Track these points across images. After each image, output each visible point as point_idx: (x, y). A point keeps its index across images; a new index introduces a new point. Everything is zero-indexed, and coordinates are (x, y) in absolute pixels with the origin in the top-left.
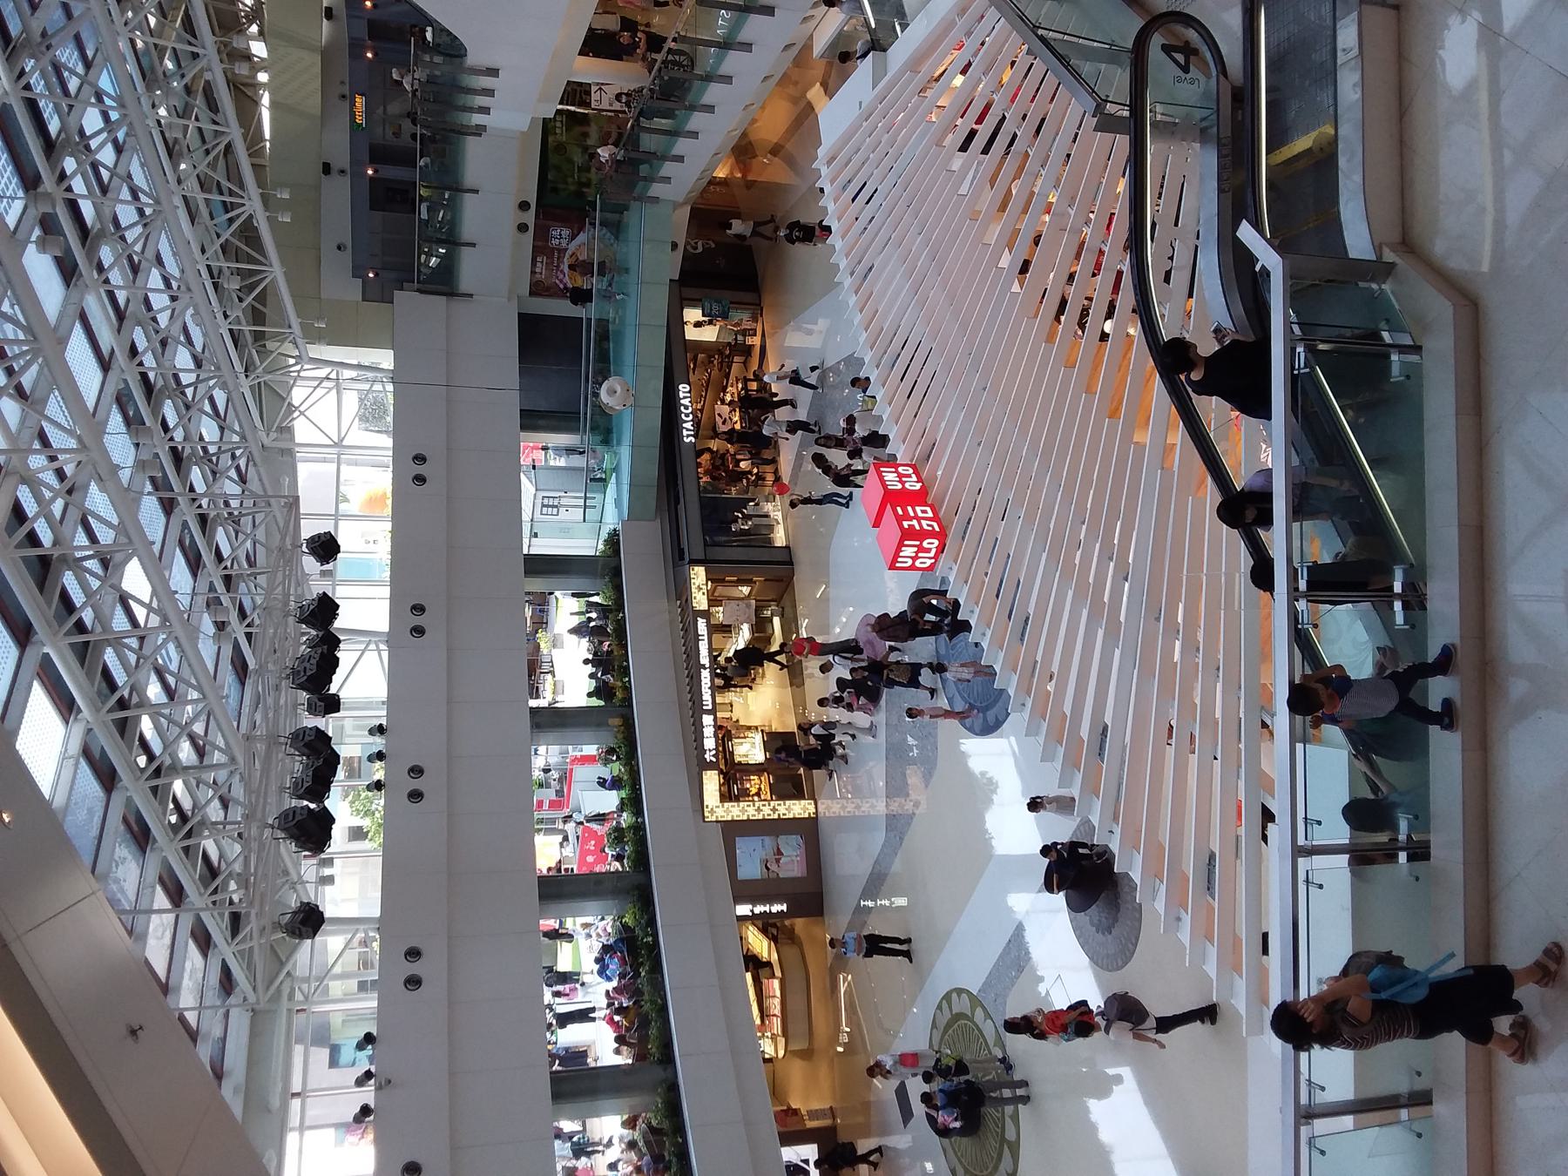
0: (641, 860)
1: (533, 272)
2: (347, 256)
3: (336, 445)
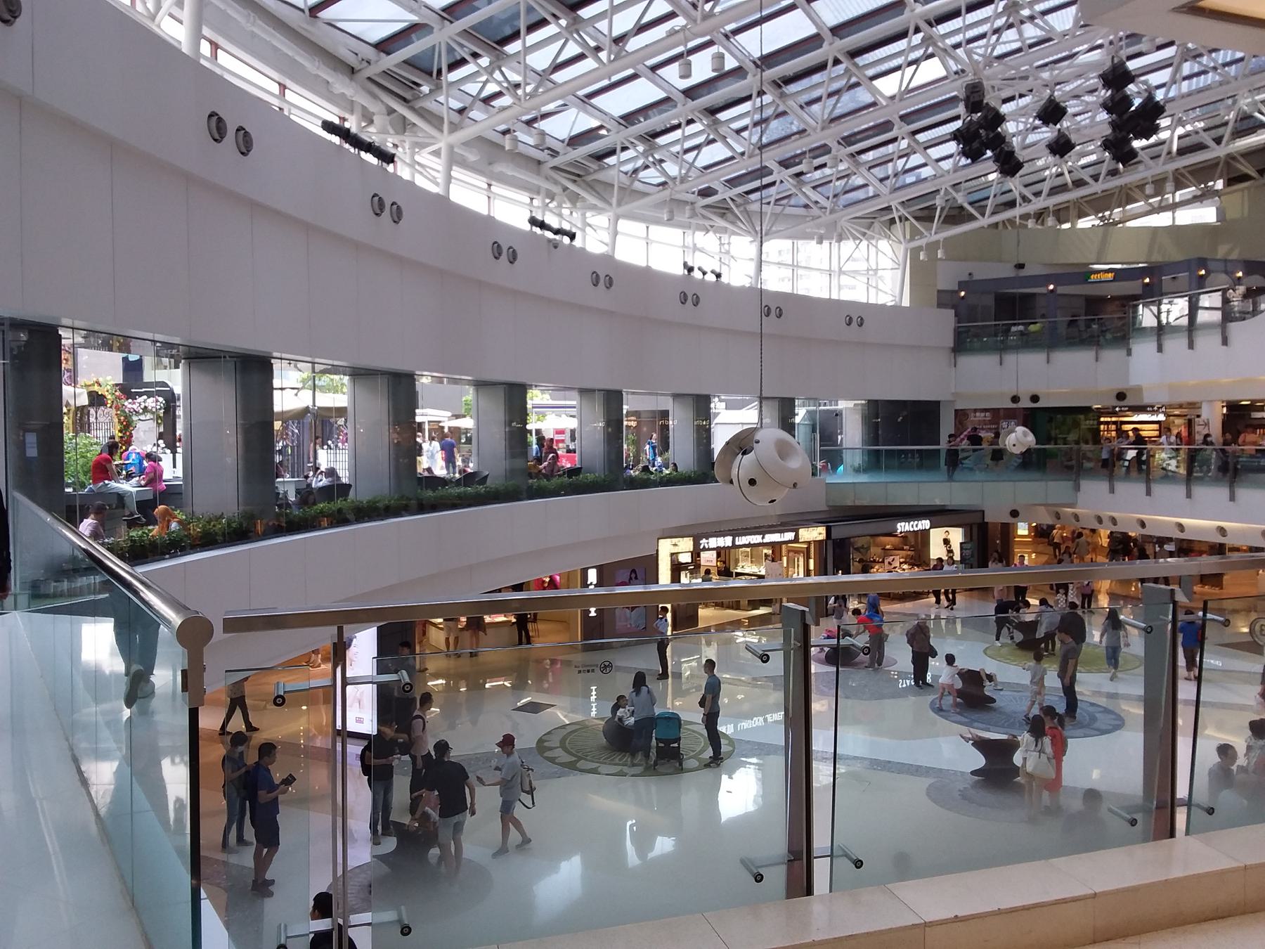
0: (633, 484)
1: (975, 411)
2: (966, 278)
3: (840, 269)
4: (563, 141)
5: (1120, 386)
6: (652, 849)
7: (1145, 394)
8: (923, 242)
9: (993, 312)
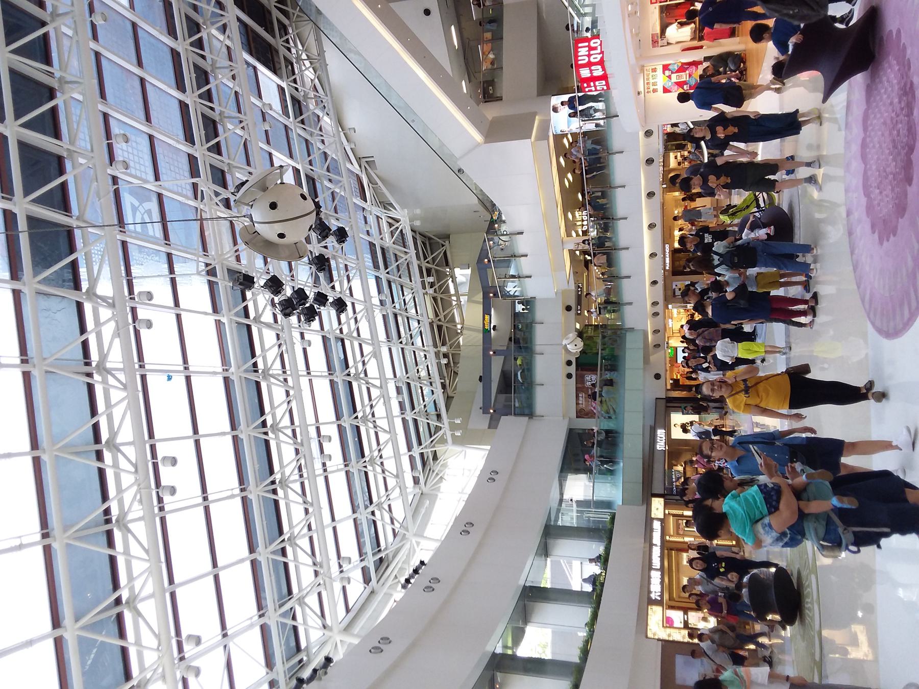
1: (577, 404)
4: (267, 673)
5: (560, 308)
6: (840, 472)
8: (449, 433)
9: (511, 392)
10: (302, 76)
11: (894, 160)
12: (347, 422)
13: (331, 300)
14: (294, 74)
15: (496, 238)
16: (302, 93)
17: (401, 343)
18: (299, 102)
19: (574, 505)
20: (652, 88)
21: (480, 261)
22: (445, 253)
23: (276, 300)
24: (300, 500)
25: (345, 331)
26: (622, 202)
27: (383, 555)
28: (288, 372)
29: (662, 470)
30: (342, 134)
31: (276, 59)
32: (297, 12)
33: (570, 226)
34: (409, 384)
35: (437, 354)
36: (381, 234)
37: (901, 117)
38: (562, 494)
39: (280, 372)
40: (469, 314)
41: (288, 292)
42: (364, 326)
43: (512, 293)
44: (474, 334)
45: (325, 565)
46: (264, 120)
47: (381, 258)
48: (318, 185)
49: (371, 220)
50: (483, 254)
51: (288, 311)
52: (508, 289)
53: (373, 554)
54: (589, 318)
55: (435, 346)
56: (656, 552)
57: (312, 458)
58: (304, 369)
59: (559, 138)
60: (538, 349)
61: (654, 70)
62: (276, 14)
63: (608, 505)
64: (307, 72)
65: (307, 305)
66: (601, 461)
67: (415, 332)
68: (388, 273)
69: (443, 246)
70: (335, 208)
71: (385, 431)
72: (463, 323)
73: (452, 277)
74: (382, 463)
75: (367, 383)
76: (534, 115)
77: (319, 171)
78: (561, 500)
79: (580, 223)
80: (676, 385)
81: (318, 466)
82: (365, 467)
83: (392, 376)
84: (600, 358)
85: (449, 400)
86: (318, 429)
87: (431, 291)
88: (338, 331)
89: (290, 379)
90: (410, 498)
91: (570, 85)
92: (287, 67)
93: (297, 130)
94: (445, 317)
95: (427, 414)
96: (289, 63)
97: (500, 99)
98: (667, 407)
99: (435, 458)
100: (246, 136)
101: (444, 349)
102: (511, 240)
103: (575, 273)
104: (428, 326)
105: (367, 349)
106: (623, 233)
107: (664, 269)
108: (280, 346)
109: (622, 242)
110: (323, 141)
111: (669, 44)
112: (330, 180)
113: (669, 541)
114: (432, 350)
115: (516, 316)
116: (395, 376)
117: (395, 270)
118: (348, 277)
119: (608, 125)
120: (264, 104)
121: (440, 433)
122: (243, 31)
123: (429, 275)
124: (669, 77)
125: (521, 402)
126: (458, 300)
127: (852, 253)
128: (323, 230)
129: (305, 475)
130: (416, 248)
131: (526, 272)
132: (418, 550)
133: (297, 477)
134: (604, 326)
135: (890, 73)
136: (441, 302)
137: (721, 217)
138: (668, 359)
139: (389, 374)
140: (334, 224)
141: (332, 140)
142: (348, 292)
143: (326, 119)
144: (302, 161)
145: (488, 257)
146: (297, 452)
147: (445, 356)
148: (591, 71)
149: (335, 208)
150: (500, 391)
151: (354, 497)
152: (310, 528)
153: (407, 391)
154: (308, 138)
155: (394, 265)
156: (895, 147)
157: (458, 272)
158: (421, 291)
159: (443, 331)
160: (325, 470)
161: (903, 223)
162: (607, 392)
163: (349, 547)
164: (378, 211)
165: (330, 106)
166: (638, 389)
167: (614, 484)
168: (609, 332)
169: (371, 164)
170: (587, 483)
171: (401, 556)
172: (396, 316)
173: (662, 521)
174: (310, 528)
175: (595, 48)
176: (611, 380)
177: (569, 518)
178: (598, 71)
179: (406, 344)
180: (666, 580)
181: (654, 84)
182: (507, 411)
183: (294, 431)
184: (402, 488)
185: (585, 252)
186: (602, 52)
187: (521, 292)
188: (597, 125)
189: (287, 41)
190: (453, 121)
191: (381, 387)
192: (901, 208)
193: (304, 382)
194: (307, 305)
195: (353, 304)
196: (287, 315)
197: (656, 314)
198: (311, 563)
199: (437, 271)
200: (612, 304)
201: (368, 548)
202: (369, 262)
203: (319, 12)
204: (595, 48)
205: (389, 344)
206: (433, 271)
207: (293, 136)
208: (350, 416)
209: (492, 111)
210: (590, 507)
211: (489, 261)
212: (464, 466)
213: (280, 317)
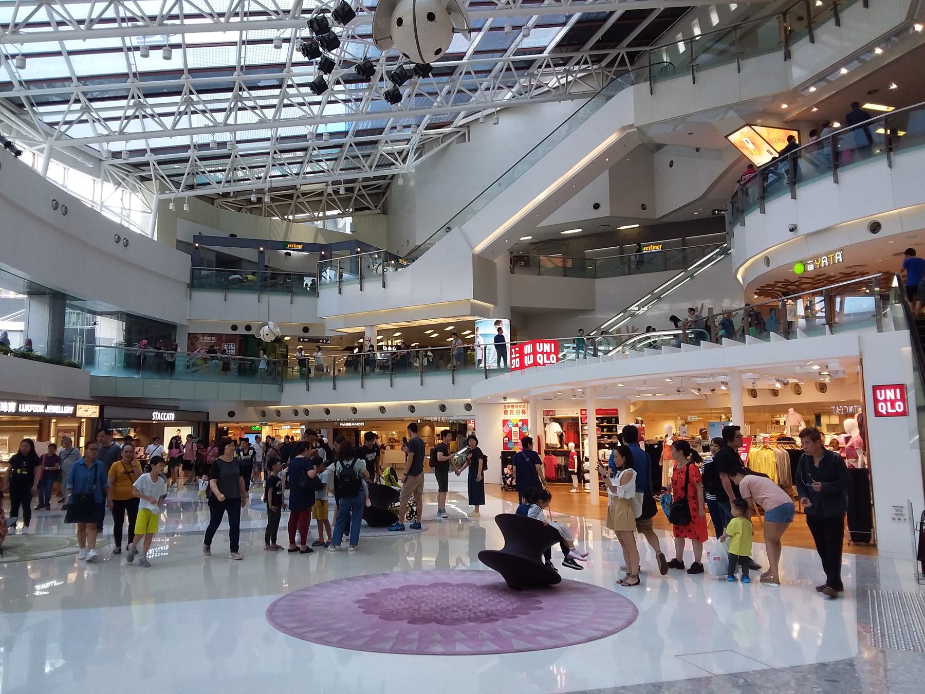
1: (204, 335)
3: (102, 203)
5: (306, 321)
7: (328, 327)
8: (172, 196)
9: (217, 265)
10: (551, 74)
11: (431, 609)
12: (185, 81)
13: (325, 77)
14: (555, 65)
15: (380, 261)
16: (535, 72)
17: (275, 153)
18: (528, 68)
19: (89, 327)
20: (509, 410)
21: (359, 244)
22: (368, 208)
23: (328, 15)
24: (95, 15)
25: (291, 91)
26: (407, 383)
27: (27, 108)
28: (245, 19)
29: (131, 416)
30: (494, 110)
31: (571, 48)
32: (611, 75)
33: (387, 334)
34: (228, 156)
35: (261, 191)
36: (392, 141)
37: (468, 613)
38: (101, 314)
39: (246, 9)
40: (304, 228)
41: (337, 30)
42: (295, 112)
43: (324, 274)
44: (282, 233)
45: (15, 37)
46: (514, 28)
47: (367, 139)
48: (445, 78)
49: (407, 133)
50: (366, 247)
51: (315, 25)
52: (328, 271)
53: (27, 97)
54: (295, 350)
55: (271, 190)
56: (38, 408)
57: (145, 35)
58: (250, 38)
59: (472, 326)
60: (265, 297)
61: (524, 412)
62: (613, 53)
63: (91, 359)
64: (555, 79)
65: (321, 49)
66: (140, 356)
67: (287, 169)
68: (351, 145)
69: (376, 207)
70: (421, 95)
71: (175, 124)
72: (294, 221)
73: (343, 213)
74: (137, 117)
75: (231, 110)
76: (495, 303)
77: (460, 81)
78: (94, 313)
79: (390, 343)
80: (222, 433)
81: (135, 41)
82: (133, 97)
83: (238, 139)
84: (249, 357)
85: (210, 199)
86: (178, 46)
87: (330, 190)
88: (290, 82)
89: (237, 19)
90: (95, 146)
91: (518, 338)
92: (562, 59)
93: (501, 62)
94: (302, 203)
95: (194, 174)
96: (566, 61)
97: (512, 272)
98: (199, 423)
99: (143, 179)
100: (500, 5)
101: (267, 199)
102: (377, 275)
103: (341, 338)
104: (293, 183)
105: (269, 113)
106: (377, 384)
107: (340, 422)
108: (276, 12)
109: (369, 383)
110: (488, 89)
111: (545, 425)
112: (449, 92)
113: (50, 422)
114: (266, 186)
115: (300, 277)
116: (238, 142)
117: (353, 154)
118: (349, 101)
119: (479, 371)
120: (529, 29)
121: (173, 188)
122: (600, 16)
123: (347, 189)
124: (517, 425)
125: (207, 276)
126: (319, 219)
127: (349, 579)
128: (399, 77)
129: (124, 25)
130: (376, 178)
131: (345, 288)
132: (34, 149)
133: (122, 15)
134: (286, 364)
135: (506, 603)
136: (319, 201)
137: (388, 469)
138: (249, 425)
139: (240, 135)
140: (405, 91)
141: (489, 99)
142: (333, 99)
143: (510, 95)
144: (471, 64)
145: (362, 251)
146: (152, 18)
147: (260, 200)
148: (529, 354)
149: (421, 95)
150: (219, 255)
151: (97, 81)
152: (60, 24)
153: (220, 154)
154: (493, 74)
155: (358, 153)
156: (442, 609)
157: (349, 220)
158: (330, 180)
159: (286, 199)
160: (129, 49)
161: (375, 618)
162: (217, 365)
163: (36, 69)
164: (415, 140)
165: (520, 101)
166: (219, 396)
167: (113, 368)
168: (279, 369)
169: (463, 138)
170: (114, 342)
171: (26, 130)
172: (304, 149)
173: (73, 415)
174: (60, 24)
175: (548, 359)
176: (229, 369)
177: (73, 321)
178: (528, 361)
179: (273, 158)
180: (24, 419)
181: (512, 412)
182: (197, 262)
183: (176, 17)
184: (109, 138)
185: (361, 347)
186: (544, 364)
187: (325, 284)
188: (480, 361)
189: (586, 62)
190: (496, 226)
191: (226, 125)
192: (387, 616)
193: (233, 36)
194: (321, 49)
195: (319, 103)
196: (311, 24)
197: (296, 413)
198: (17, 21)
199: (351, 198)
200: (306, 373)
201: (34, 92)
202: (363, 126)
203: (609, 98)
204: (548, 359)
205: (274, 139)
206: (351, 194)
207: (496, 58)
208: (193, 85)
209: (501, 262)
210: (88, 342)
211: (358, 253)
212: (131, 209)
213: (308, 16)
